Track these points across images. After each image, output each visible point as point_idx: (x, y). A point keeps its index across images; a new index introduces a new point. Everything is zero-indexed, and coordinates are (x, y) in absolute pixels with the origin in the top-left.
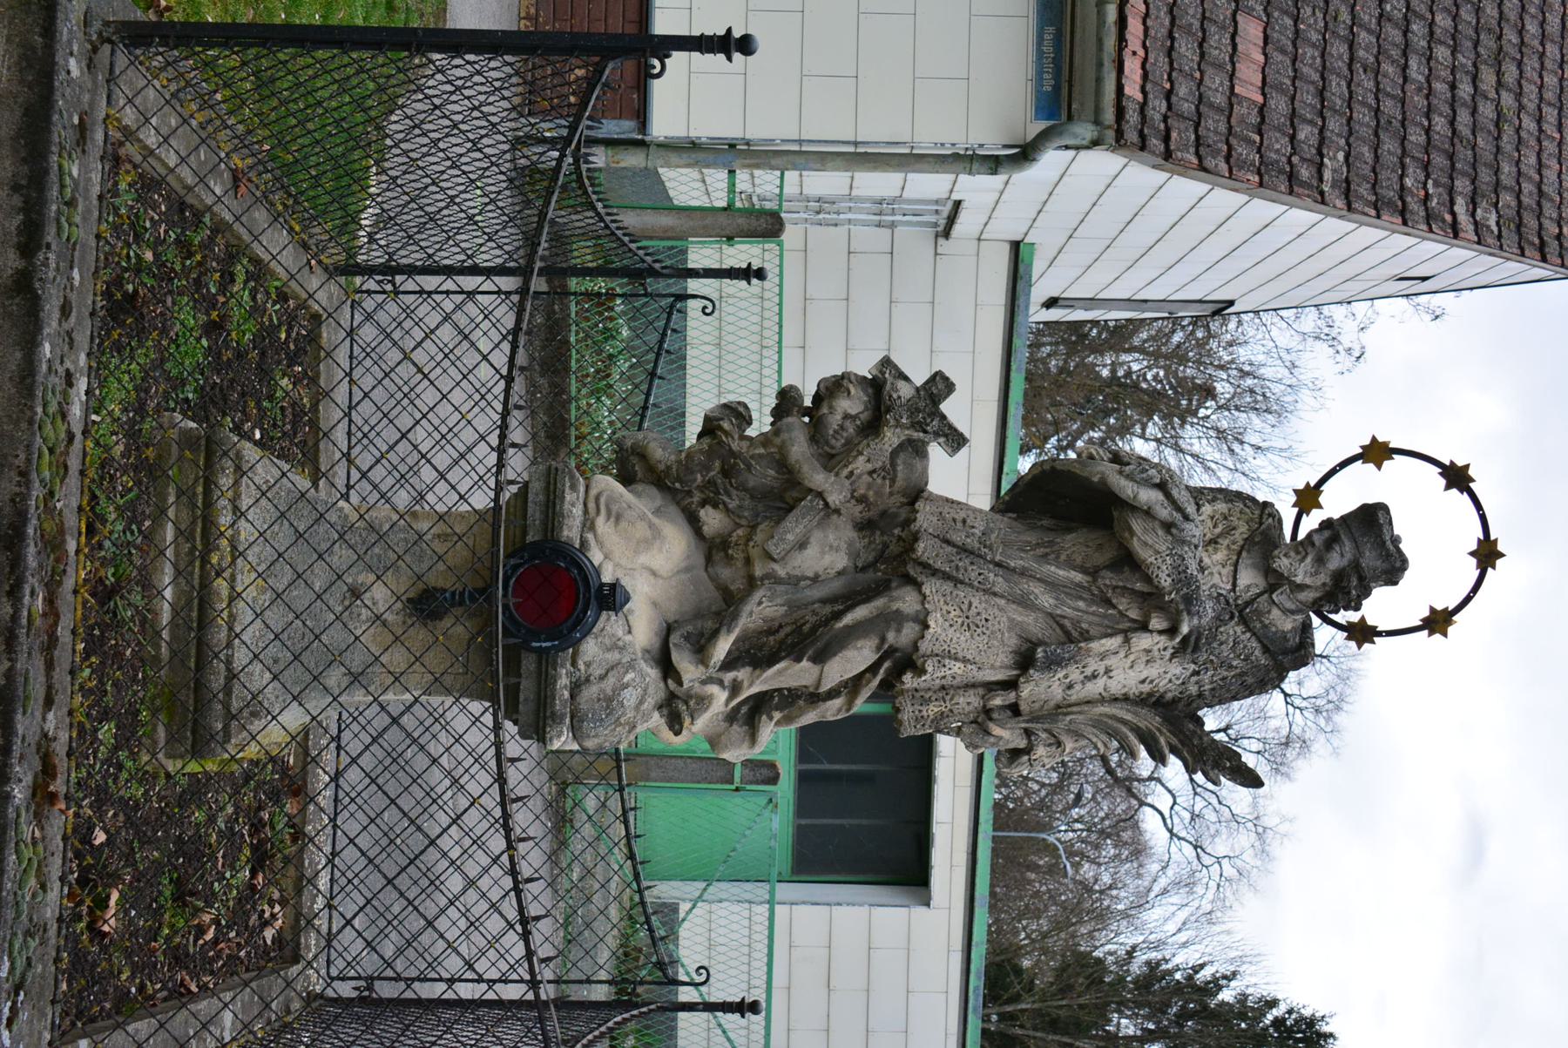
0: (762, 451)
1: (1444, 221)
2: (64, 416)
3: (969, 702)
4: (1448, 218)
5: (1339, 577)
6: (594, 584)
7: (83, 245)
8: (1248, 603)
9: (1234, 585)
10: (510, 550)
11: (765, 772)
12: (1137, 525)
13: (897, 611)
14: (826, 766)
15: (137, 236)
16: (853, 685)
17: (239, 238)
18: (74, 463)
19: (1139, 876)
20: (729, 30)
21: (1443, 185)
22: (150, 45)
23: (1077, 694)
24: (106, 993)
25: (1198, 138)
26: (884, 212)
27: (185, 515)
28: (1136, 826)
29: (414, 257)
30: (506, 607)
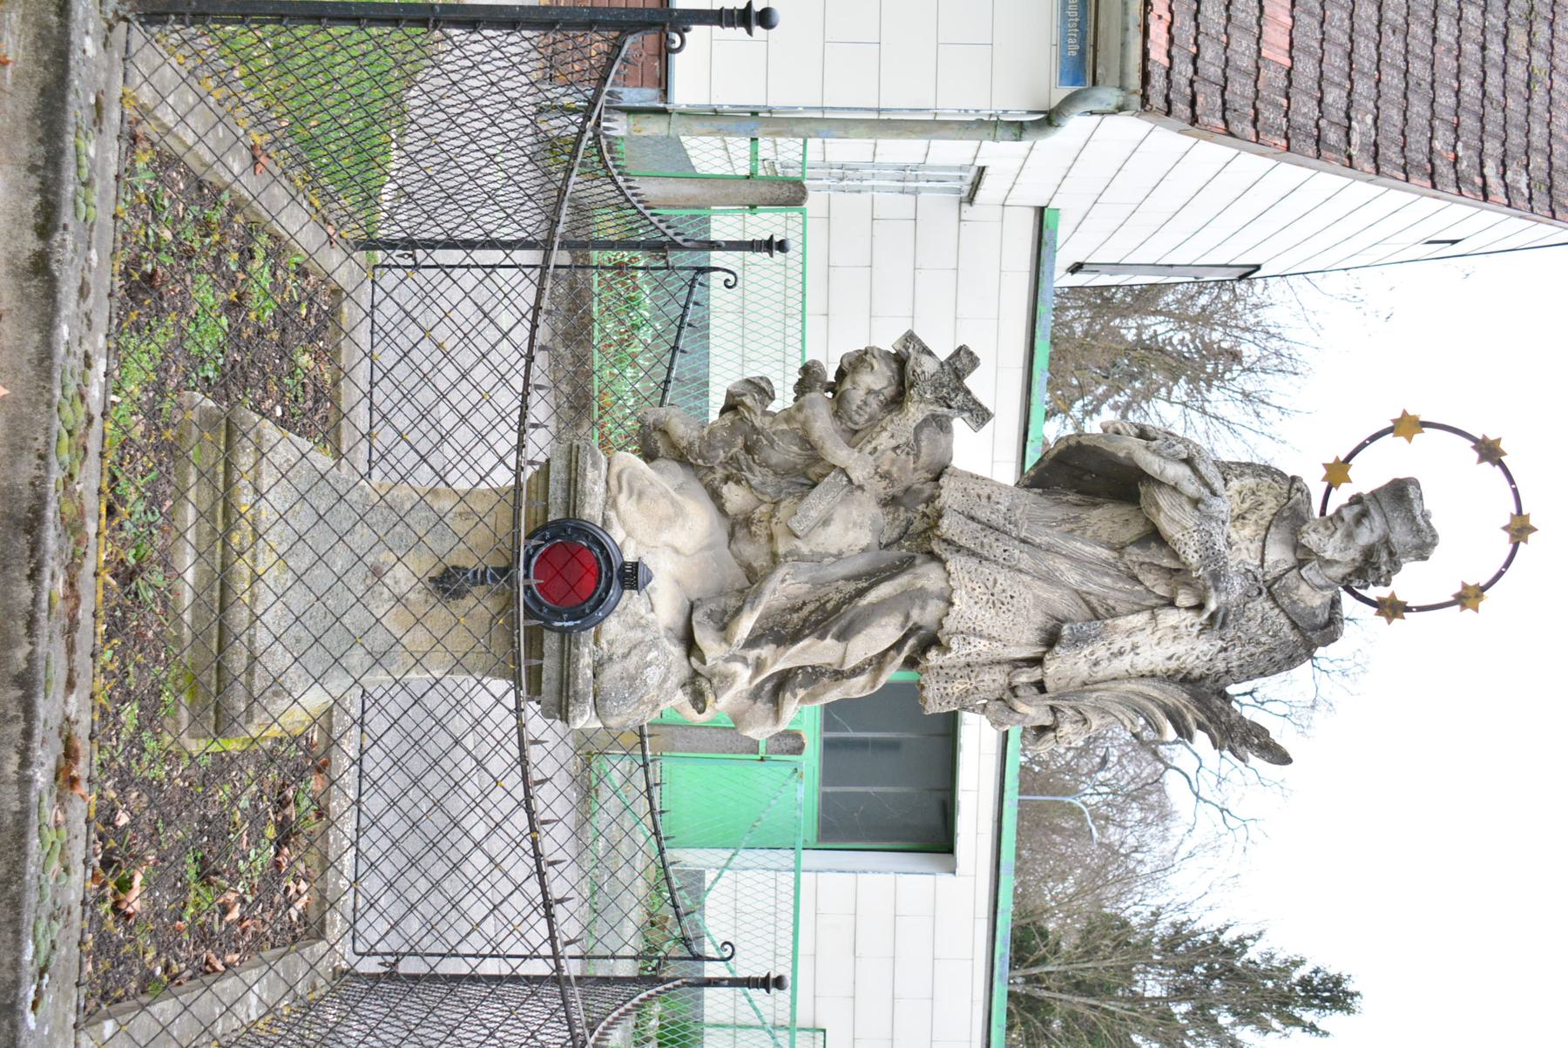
0: (785, 427)
1: (1473, 184)
2: (83, 398)
3: (994, 680)
4: (1478, 180)
5: (1369, 553)
6: (616, 565)
7: (101, 225)
8: (1276, 580)
9: (1263, 561)
10: (532, 528)
11: (792, 743)
12: (1164, 499)
13: (922, 588)
14: (851, 734)
15: (155, 218)
16: (880, 661)
17: (258, 215)
18: (94, 446)
19: (1164, 839)
20: (749, 4)
21: (1473, 148)
22: (165, 23)
23: (1104, 671)
24: (131, 973)
25: (1224, 103)
26: (908, 179)
27: (206, 493)
28: (1161, 791)
29: (435, 233)
30: (528, 588)
